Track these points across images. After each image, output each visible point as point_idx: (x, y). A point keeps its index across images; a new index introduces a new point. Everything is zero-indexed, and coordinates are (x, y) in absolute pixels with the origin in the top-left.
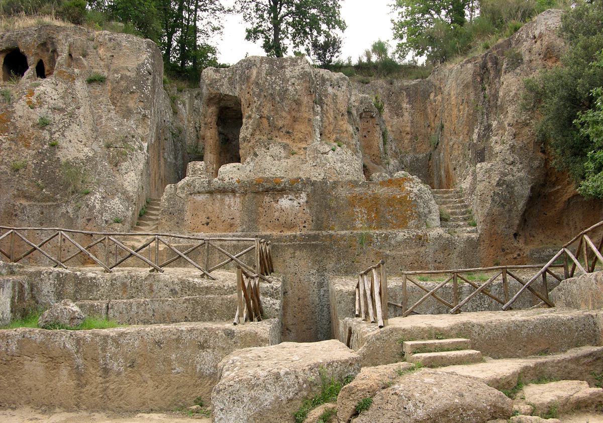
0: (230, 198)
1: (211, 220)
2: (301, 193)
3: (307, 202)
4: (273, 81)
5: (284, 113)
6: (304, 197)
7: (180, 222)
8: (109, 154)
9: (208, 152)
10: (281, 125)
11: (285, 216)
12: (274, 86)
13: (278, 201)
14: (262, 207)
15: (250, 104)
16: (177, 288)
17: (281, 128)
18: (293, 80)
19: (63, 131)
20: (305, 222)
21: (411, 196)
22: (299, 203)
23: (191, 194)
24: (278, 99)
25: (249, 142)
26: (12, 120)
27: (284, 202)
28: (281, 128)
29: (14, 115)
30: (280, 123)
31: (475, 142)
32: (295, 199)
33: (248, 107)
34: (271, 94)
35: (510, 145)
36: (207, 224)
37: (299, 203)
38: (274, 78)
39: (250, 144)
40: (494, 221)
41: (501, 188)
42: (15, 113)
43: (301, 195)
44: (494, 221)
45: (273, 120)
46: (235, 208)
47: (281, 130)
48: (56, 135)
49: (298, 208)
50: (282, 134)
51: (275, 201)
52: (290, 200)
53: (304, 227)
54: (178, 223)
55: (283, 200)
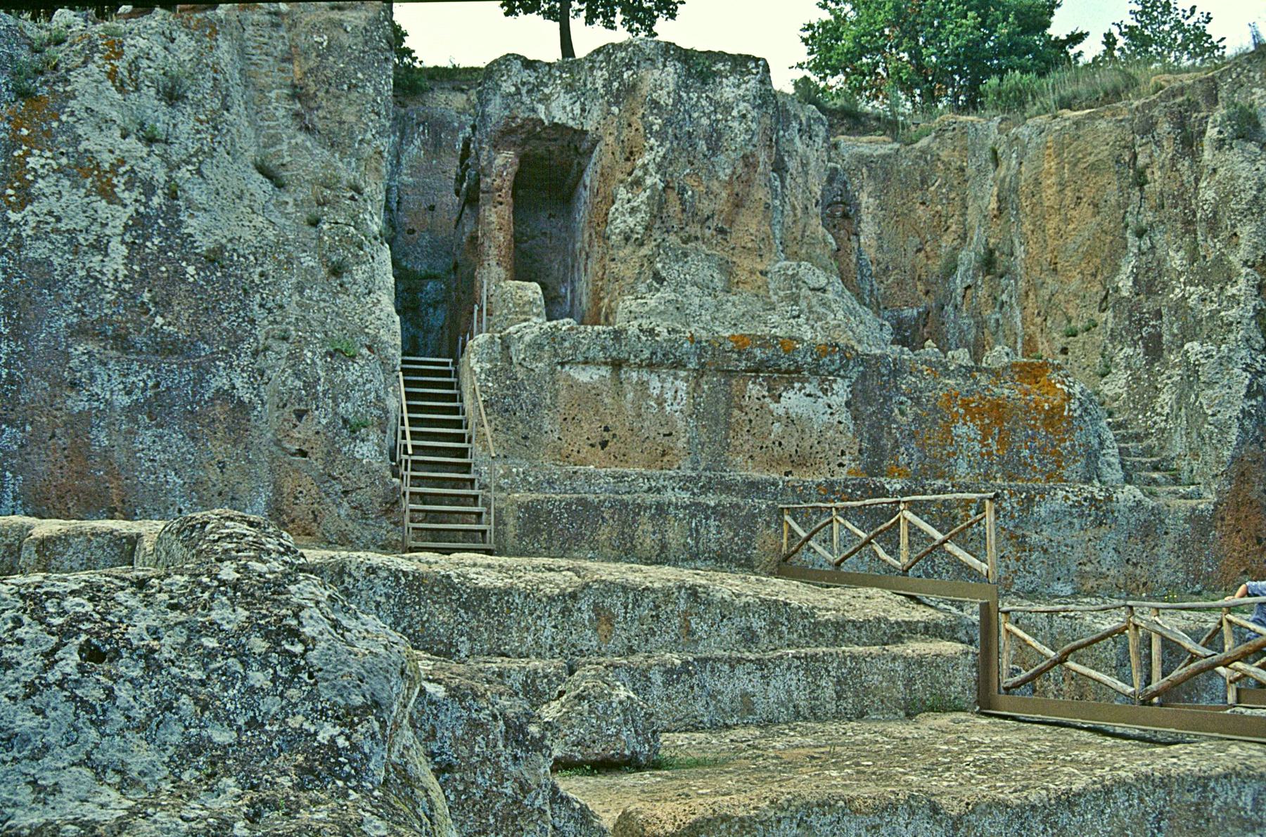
0: (663, 381)
1: (614, 436)
2: (835, 381)
3: (848, 404)
4: (693, 102)
5: (716, 183)
6: (841, 390)
7: (531, 435)
8: (320, 239)
9: (493, 263)
10: (707, 213)
11: (796, 435)
12: (695, 115)
13: (780, 396)
14: (741, 409)
15: (631, 153)
16: (758, 624)
17: (708, 218)
18: (743, 106)
19: (200, 163)
20: (843, 453)
21: (1073, 407)
22: (830, 406)
23: (563, 364)
24: (702, 146)
25: (642, 244)
26: (64, 118)
27: (793, 401)
28: (708, 218)
29: (72, 103)
30: (705, 207)
31: (1125, 294)
32: (820, 394)
33: (628, 159)
34: (689, 134)
35: (1254, 308)
36: (604, 444)
37: (830, 406)
38: (694, 96)
39: (645, 251)
40: (1243, 474)
41: (1254, 403)
42: (75, 97)
43: (834, 386)
44: (1243, 474)
45: (692, 197)
46: (676, 407)
47: (708, 223)
48: (184, 173)
49: (826, 417)
50: (708, 233)
51: (771, 396)
52: (810, 395)
53: (841, 465)
54: (526, 438)
55: (791, 394)
